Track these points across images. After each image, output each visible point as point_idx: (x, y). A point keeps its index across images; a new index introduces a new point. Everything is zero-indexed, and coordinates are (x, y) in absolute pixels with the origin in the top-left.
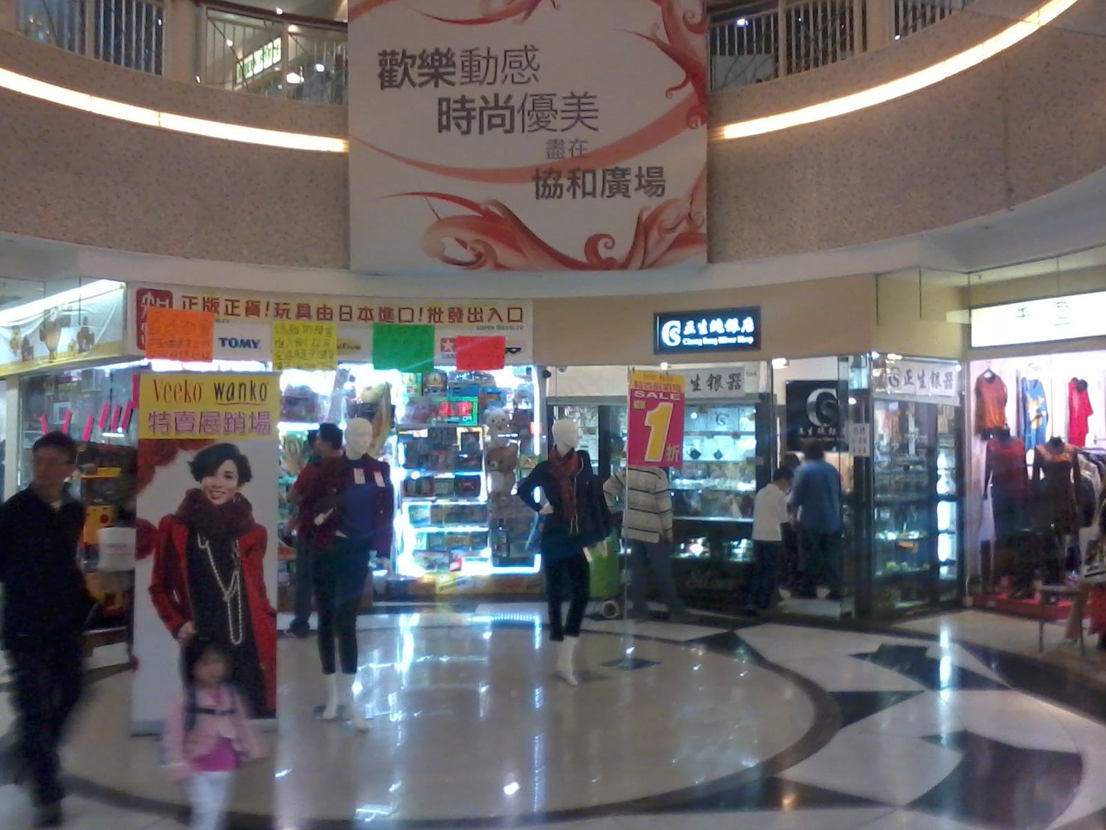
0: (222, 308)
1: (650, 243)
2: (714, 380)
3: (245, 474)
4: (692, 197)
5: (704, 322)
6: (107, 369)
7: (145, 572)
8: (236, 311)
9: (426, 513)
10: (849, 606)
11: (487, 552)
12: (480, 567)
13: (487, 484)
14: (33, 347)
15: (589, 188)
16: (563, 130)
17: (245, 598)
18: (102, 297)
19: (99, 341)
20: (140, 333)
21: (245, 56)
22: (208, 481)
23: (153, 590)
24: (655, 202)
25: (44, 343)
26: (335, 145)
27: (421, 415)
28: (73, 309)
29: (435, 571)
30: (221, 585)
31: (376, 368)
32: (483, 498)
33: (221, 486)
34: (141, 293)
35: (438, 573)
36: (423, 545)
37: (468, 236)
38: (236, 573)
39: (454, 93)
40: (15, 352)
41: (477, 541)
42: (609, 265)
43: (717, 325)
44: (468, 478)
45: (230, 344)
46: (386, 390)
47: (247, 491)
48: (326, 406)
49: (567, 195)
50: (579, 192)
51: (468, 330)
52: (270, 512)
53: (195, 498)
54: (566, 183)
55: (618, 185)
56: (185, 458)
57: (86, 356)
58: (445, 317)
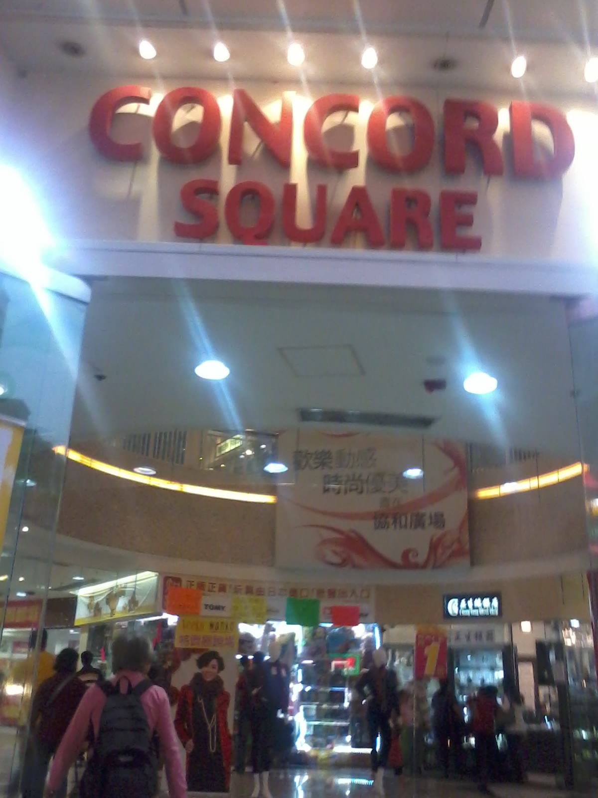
0: (206, 588)
1: (439, 555)
2: (478, 636)
3: (221, 667)
4: (461, 528)
5: (479, 600)
6: (143, 621)
7: (171, 713)
8: (214, 589)
9: (313, 712)
10: (561, 779)
11: (348, 738)
12: (344, 748)
13: (348, 695)
14: (101, 608)
15: (403, 523)
16: (390, 492)
17: (218, 727)
18: (147, 578)
19: (143, 603)
20: (164, 600)
21: (222, 442)
22: (205, 669)
23: (176, 722)
24: (439, 533)
25: (108, 606)
26: (269, 499)
27: (311, 652)
28: (128, 586)
29: (318, 748)
30: (207, 721)
31: (288, 624)
32: (346, 704)
33: (210, 672)
34: (166, 579)
35: (319, 750)
36: (311, 732)
37: (339, 549)
38: (214, 716)
39: (332, 473)
40: (90, 611)
41: (343, 731)
42: (416, 566)
43: (478, 602)
44: (337, 692)
45: (210, 607)
46: (292, 636)
47: (222, 675)
48: (259, 647)
49: (392, 527)
50: (398, 526)
51: (338, 603)
52: (230, 681)
53: (198, 678)
54: (391, 520)
55: (419, 522)
56: (195, 657)
57: (134, 613)
58: (326, 594)
